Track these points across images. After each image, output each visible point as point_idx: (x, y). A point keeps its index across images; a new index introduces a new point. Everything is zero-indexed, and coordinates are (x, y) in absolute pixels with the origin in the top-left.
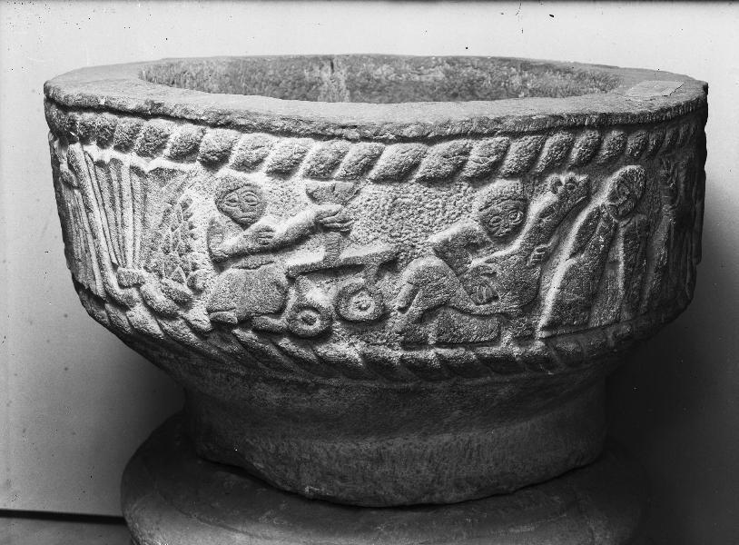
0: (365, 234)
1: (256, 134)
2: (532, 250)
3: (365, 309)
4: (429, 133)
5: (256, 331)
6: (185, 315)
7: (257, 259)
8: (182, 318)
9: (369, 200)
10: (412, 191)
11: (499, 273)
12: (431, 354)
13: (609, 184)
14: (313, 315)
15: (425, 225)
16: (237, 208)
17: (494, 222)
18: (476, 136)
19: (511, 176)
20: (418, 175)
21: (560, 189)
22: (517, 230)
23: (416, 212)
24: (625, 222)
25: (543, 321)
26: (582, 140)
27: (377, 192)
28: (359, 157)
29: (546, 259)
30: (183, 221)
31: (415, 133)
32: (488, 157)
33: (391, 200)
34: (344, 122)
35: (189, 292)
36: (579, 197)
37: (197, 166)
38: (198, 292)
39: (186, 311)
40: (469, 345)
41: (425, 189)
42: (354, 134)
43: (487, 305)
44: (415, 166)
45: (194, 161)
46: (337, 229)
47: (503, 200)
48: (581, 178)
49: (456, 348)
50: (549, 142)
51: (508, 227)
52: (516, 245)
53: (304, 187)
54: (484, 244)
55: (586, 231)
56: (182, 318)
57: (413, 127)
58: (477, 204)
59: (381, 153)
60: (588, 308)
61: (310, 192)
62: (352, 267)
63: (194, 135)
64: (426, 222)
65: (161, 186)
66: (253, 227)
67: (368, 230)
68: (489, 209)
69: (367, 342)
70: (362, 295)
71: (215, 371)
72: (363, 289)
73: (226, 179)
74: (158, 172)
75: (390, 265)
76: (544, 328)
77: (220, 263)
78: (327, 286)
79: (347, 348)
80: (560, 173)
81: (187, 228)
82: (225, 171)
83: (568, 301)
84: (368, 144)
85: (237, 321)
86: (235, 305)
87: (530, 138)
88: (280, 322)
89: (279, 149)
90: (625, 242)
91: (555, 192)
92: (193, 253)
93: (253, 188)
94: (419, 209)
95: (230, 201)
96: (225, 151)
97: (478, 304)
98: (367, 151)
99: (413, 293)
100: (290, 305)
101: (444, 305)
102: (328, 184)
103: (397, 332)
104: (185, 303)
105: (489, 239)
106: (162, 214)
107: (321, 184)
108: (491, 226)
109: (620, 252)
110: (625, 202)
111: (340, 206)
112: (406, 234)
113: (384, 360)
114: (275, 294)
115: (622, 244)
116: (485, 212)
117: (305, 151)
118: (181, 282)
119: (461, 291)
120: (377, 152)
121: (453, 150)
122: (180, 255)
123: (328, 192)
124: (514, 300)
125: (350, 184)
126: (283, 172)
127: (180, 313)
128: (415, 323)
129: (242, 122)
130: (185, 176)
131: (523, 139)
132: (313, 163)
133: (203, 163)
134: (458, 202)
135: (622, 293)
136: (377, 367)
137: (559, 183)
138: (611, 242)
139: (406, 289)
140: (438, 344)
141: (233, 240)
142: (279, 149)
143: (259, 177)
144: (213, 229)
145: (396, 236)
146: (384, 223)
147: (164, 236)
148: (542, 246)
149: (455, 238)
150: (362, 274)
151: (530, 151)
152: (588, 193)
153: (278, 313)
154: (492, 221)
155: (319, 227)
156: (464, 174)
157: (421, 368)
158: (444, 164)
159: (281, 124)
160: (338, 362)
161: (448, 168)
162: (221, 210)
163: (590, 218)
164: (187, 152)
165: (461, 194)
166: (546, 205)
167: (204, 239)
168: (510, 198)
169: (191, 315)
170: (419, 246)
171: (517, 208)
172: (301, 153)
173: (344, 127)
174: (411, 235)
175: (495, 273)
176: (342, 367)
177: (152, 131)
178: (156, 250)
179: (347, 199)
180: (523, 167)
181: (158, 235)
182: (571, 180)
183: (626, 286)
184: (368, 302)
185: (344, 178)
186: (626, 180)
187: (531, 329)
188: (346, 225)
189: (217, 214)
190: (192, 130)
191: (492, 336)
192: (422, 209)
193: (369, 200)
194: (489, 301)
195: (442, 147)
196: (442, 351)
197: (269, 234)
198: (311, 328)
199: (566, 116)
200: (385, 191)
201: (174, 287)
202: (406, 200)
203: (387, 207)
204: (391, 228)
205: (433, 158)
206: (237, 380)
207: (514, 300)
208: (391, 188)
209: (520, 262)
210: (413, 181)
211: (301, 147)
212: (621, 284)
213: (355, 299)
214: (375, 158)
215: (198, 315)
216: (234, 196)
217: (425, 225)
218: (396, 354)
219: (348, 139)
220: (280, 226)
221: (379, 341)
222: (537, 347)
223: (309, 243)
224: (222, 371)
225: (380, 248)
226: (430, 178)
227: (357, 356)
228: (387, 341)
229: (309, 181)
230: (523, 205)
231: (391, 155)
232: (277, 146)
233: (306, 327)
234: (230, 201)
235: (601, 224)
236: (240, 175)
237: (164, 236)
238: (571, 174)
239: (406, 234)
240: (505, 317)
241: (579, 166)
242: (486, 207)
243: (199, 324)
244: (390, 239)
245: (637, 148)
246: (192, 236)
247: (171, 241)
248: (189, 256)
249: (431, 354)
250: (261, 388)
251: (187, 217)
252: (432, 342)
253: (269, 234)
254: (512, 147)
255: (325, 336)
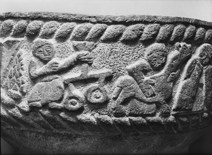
0: (99, 65)
1: (51, 22)
2: (169, 75)
3: (98, 98)
4: (126, 20)
5: (50, 109)
6: (18, 105)
7: (51, 77)
8: (17, 107)
9: (100, 50)
10: (119, 46)
11: (156, 84)
12: (126, 119)
13: (199, 50)
14: (76, 101)
15: (124, 61)
16: (43, 54)
17: (154, 61)
18: (146, 23)
19: (160, 41)
20: (122, 39)
21: (180, 49)
22: (163, 65)
23: (121, 55)
24: (205, 67)
25: (174, 107)
26: (189, 29)
27: (104, 46)
28: (97, 30)
29: (175, 80)
30: (18, 63)
31: (120, 20)
32: (151, 32)
33: (110, 50)
34: (90, 15)
35: (20, 94)
36: (188, 53)
37: (24, 39)
38: (24, 94)
39: (19, 104)
40: (144, 116)
41: (125, 45)
42: (94, 20)
43: (150, 98)
44: (120, 35)
45: (23, 37)
46: (86, 62)
47: (157, 51)
48: (189, 45)
49: (138, 117)
50: (176, 28)
51: (159, 63)
52: (163, 72)
53: (72, 44)
54: (149, 71)
55: (191, 68)
56: (17, 107)
57: (120, 18)
58: (146, 53)
59: (106, 29)
60: (192, 102)
61: (75, 46)
62: (93, 79)
63: (24, 24)
64: (125, 60)
65: (9, 49)
66: (50, 62)
67: (100, 63)
68: (152, 55)
69: (99, 113)
70: (97, 92)
71: (31, 132)
72: (98, 89)
73: (38, 42)
74: (8, 42)
75: (109, 79)
76: (174, 110)
77: (34, 80)
78: (82, 88)
79: (88, 116)
80: (180, 42)
81: (20, 65)
82: (37, 39)
83: (184, 98)
84: (100, 25)
85: (41, 106)
86: (41, 98)
87: (168, 26)
88: (60, 105)
89: (61, 28)
90: (206, 76)
91: (178, 50)
92: (22, 77)
93: (49, 46)
94: (122, 54)
95: (39, 51)
96: (37, 30)
97: (147, 97)
98: (100, 28)
99: (120, 91)
100: (65, 97)
101: (133, 97)
102: (83, 42)
103: (113, 109)
104: (18, 100)
105: (151, 68)
106: (9, 61)
107: (80, 42)
108: (153, 63)
109: (203, 80)
110: (205, 58)
111: (88, 52)
112: (117, 65)
113: (107, 121)
114: (59, 92)
115: (204, 77)
116: (150, 56)
117: (73, 28)
118: (17, 90)
119: (140, 91)
120: (104, 28)
121: (137, 28)
122: (17, 78)
123: (83, 45)
124: (162, 96)
125: (92, 43)
126: (63, 38)
127: (16, 104)
128: (120, 104)
129: (45, 16)
130: (19, 43)
131: (165, 25)
132: (76, 33)
133: (27, 36)
134: (138, 52)
135: (204, 98)
136: (102, 124)
137: (180, 46)
138: (201, 75)
139: (117, 89)
140: (131, 115)
141: (40, 69)
142: (61, 28)
143: (52, 41)
144: (31, 65)
145: (112, 66)
146: (107, 60)
147: (10, 71)
148: (173, 73)
149: (138, 67)
150: (97, 82)
151: (168, 31)
152: (192, 52)
153: (60, 101)
154: (153, 60)
155: (79, 62)
156: (141, 39)
157: (123, 124)
158: (133, 34)
159: (62, 16)
160: (87, 122)
161: (135, 36)
162: (35, 56)
163: (192, 64)
164: (21, 32)
165: (140, 48)
166: (175, 55)
167: (27, 70)
168: (160, 51)
169: (20, 105)
170: (122, 70)
171: (163, 55)
172: (71, 29)
173: (90, 17)
174: (119, 65)
175: (154, 84)
176: (88, 124)
177: (6, 25)
178: (6, 77)
179: (91, 49)
180: (165, 37)
181: (8, 71)
182: (184, 46)
183: (206, 94)
184: (100, 95)
185: (90, 40)
186: (205, 49)
187: (169, 110)
188: (90, 60)
189: (33, 59)
190: (23, 22)
191: (153, 111)
192: (123, 54)
193: (100, 50)
194: (152, 96)
195: (132, 27)
196: (134, 118)
197: (57, 65)
198: (75, 107)
199: (182, 18)
200: (106, 47)
201: (13, 92)
202: (116, 50)
203: (108, 53)
204: (110, 62)
205: (128, 31)
206: (41, 136)
207: (162, 96)
208: (110, 45)
209: (164, 79)
210: (119, 41)
211: (71, 26)
212: (204, 94)
213: (94, 93)
214: (103, 31)
215: (24, 105)
216: (41, 49)
217: (124, 61)
218: (111, 119)
219: (91, 22)
220: (62, 63)
221: (105, 113)
222: (171, 118)
223: (74, 69)
224: (34, 132)
225: (106, 71)
226: (127, 40)
227: (94, 120)
228: (108, 113)
229: (74, 42)
230: (165, 55)
231: (111, 30)
232: (61, 27)
233: (72, 106)
234: (39, 51)
235: (196, 66)
236: (44, 40)
237: (10, 71)
238: (185, 43)
239: (117, 65)
240: (158, 105)
241: (188, 40)
242: (151, 54)
243: (24, 108)
244: (109, 67)
245: (210, 36)
246: (22, 69)
247: (13, 72)
248: (20, 78)
249: (126, 119)
250: (52, 139)
251: (19, 61)
252: (127, 114)
253: (57, 65)
254: (161, 29)
255: (80, 111)
